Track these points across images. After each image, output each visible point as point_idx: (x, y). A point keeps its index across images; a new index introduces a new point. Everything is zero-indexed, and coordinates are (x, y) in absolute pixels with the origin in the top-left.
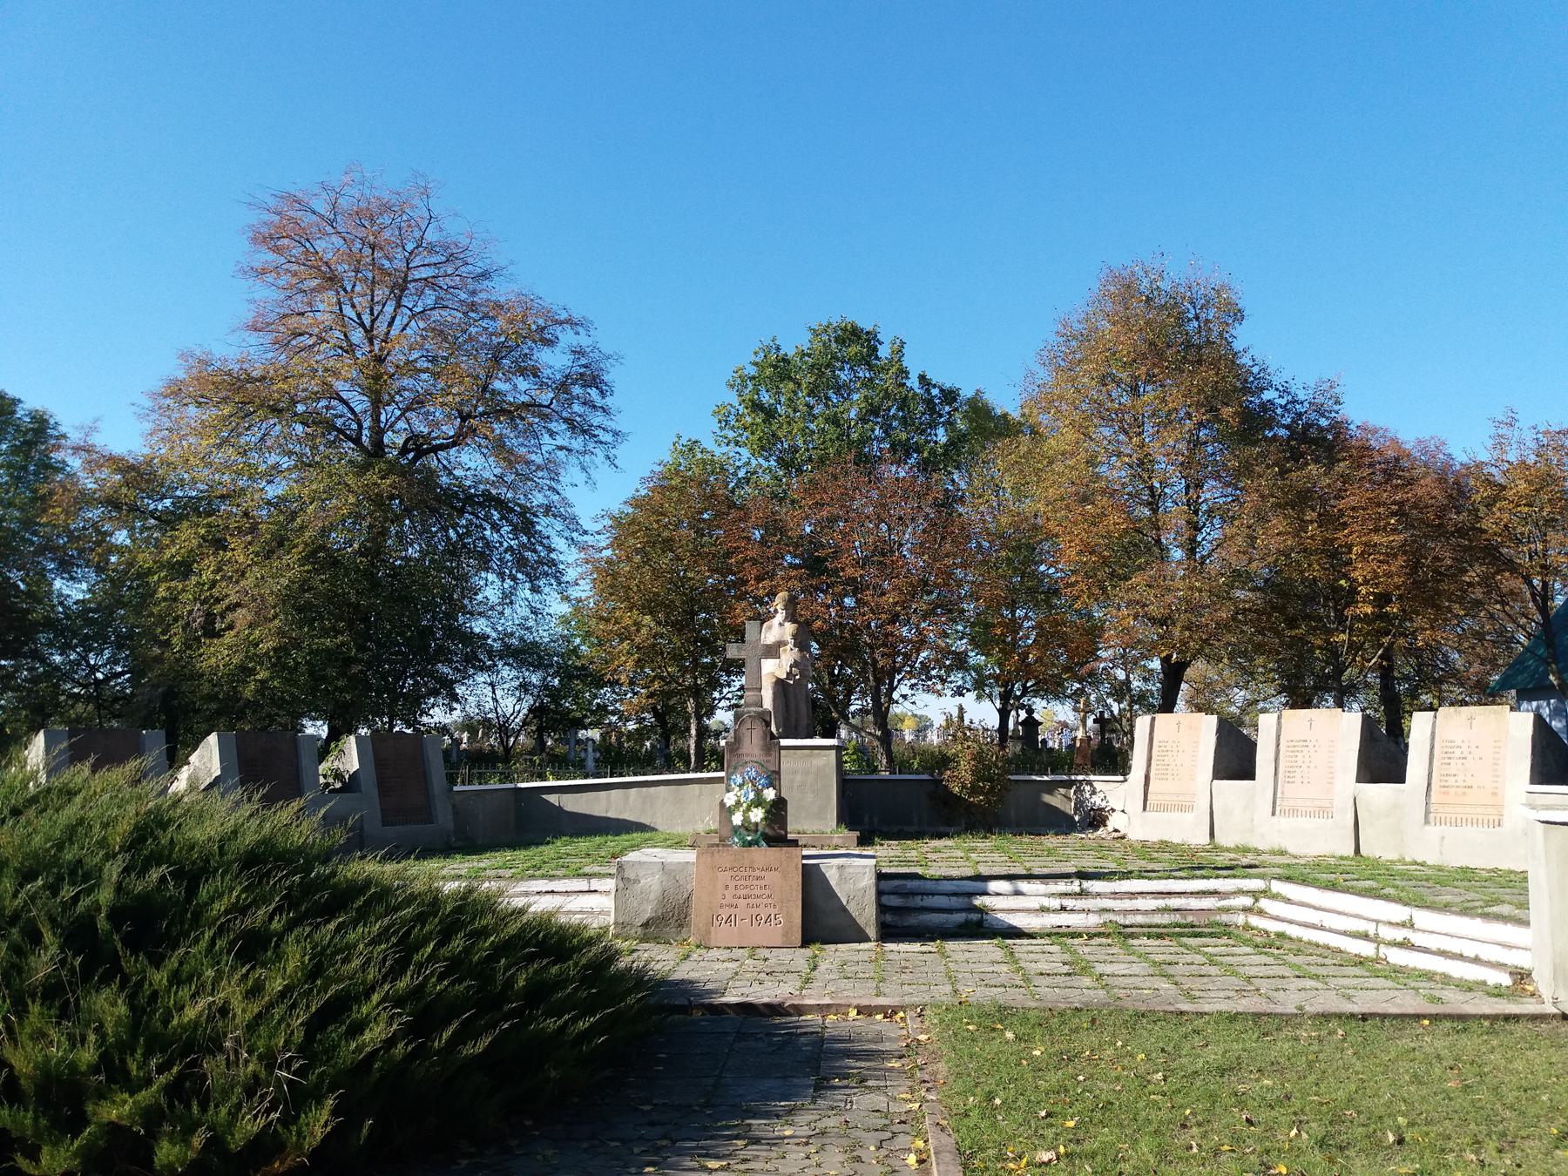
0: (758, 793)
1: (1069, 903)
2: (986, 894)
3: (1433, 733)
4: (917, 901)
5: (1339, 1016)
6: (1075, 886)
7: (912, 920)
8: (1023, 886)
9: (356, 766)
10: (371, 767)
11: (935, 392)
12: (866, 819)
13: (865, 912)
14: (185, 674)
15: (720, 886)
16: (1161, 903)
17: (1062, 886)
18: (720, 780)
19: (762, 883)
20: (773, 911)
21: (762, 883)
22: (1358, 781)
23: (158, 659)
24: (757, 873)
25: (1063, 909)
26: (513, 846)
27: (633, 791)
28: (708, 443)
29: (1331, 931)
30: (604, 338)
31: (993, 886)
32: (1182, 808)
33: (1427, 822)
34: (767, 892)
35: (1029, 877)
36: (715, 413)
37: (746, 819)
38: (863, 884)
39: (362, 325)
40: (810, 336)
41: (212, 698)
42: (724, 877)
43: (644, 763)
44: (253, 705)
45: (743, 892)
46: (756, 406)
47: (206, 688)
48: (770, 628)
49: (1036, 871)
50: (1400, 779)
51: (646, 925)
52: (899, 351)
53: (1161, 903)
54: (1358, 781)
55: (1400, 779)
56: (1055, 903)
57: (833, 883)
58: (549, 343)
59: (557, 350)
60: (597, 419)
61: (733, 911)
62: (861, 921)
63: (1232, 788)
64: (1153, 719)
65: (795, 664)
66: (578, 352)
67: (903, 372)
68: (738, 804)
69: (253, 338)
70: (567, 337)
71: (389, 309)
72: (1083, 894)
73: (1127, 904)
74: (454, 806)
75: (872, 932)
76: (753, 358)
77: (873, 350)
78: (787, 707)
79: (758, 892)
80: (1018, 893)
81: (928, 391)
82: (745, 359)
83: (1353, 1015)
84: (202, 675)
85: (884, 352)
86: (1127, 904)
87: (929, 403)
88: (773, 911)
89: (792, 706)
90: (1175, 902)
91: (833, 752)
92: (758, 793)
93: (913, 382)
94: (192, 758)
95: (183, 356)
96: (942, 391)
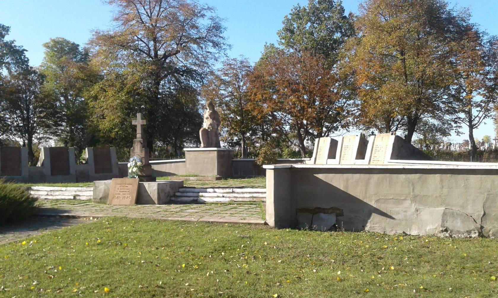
0: (136, 163)
1: (225, 195)
2: (207, 192)
3: (374, 143)
4: (185, 194)
6: (231, 190)
7: (179, 199)
8: (216, 190)
9: (87, 157)
10: (93, 158)
12: (239, 173)
13: (154, 196)
14: (96, 129)
16: (251, 195)
17: (228, 190)
18: (184, 162)
20: (129, 195)
22: (356, 158)
23: (90, 126)
25: (223, 197)
26: (120, 177)
27: (173, 164)
28: (277, 45)
30: (221, 13)
31: (208, 190)
35: (219, 188)
36: (278, 33)
37: (132, 171)
38: (154, 188)
39: (148, 16)
41: (103, 137)
42: (118, 186)
43: (172, 156)
44: (115, 139)
47: (102, 134)
49: (221, 186)
50: (335, 158)
51: (101, 199)
53: (251, 195)
54: (356, 158)
55: (335, 158)
56: (221, 195)
57: (147, 188)
58: (203, 16)
59: (206, 18)
60: (221, 41)
62: (153, 199)
65: (211, 125)
66: (212, 19)
68: (131, 166)
69: (115, 23)
70: (208, 14)
71: (157, 8)
72: (233, 192)
73: (242, 195)
74: (119, 168)
75: (156, 202)
78: (208, 138)
80: (215, 192)
82: (287, 11)
83: (209, 222)
84: (100, 131)
86: (242, 195)
90: (255, 195)
91: (216, 152)
92: (136, 163)
95: (91, 31)
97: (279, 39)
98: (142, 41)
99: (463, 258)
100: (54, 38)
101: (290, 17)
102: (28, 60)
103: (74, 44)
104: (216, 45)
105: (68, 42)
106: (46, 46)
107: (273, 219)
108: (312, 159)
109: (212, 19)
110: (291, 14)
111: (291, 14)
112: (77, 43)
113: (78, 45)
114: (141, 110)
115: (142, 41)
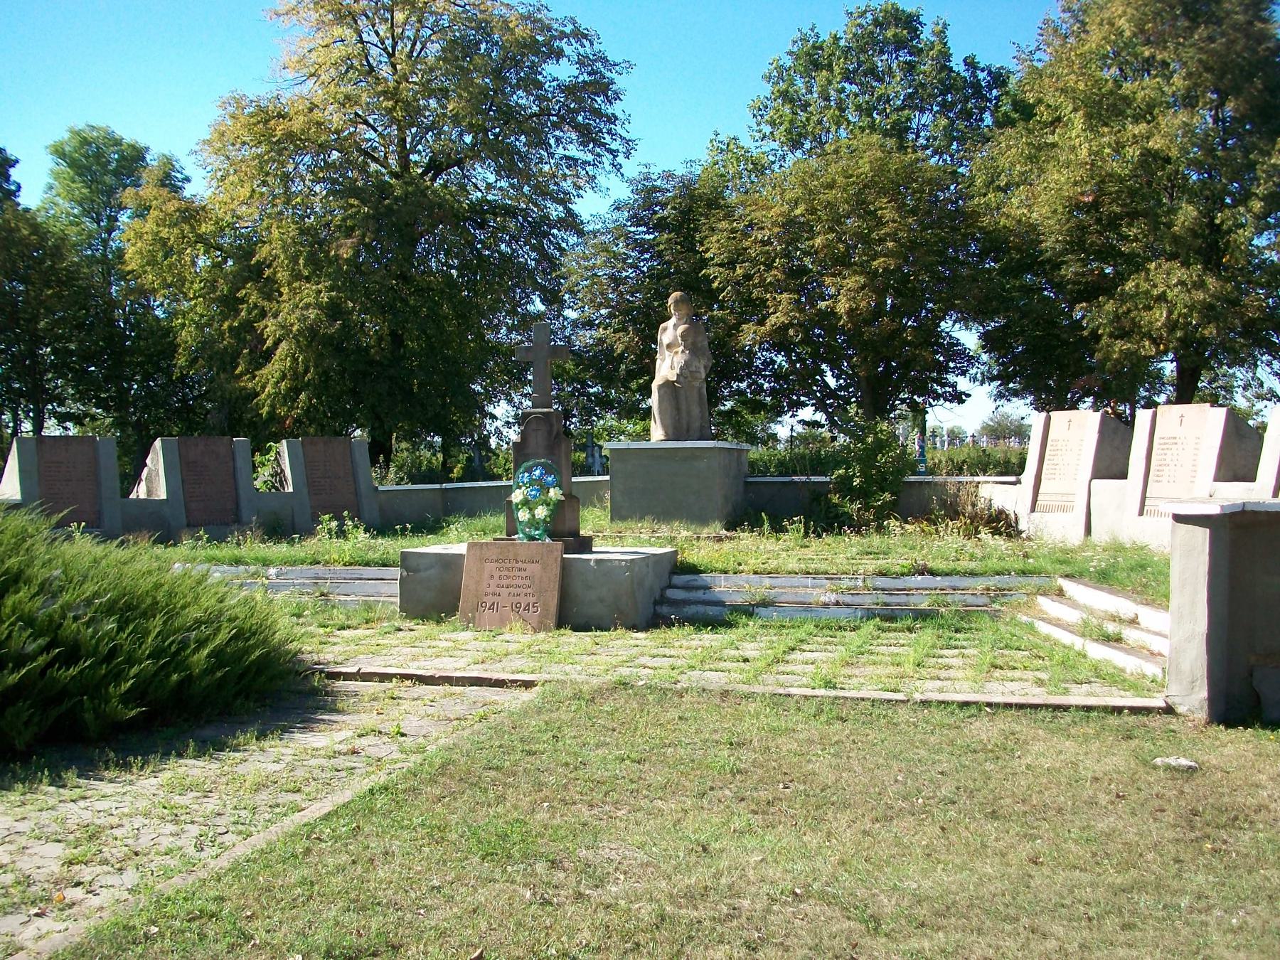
5: (1047, 706)
11: (981, 75)
15: (486, 575)
19: (523, 574)
21: (523, 574)
22: (1215, 480)
24: (520, 565)
28: (746, 142)
29: (1149, 631)
32: (1064, 509)
33: (1141, 514)
34: (528, 583)
40: (846, 19)
45: (504, 582)
46: (785, 96)
48: (665, 329)
50: (1123, 475)
52: (941, 34)
54: (1215, 480)
55: (1123, 475)
58: (559, 54)
59: (564, 61)
61: (496, 599)
63: (1105, 487)
64: (1048, 420)
67: (946, 55)
76: (789, 47)
77: (915, 33)
79: (520, 582)
81: (974, 75)
82: (779, 47)
85: (926, 34)
87: (976, 86)
88: (532, 600)
89: (684, 407)
93: (957, 64)
94: (148, 461)
96: (990, 73)
97: (753, 123)
98: (366, 122)
99: (443, 775)
100: (81, 125)
101: (788, 61)
102: (19, 187)
103: (133, 147)
104: (588, 137)
105: (118, 142)
106: (59, 152)
107: (1204, 693)
108: (1023, 477)
109: (582, 62)
110: (790, 53)
111: (790, 53)
112: (142, 142)
113: (147, 149)
114: (864, 269)
115: (366, 122)
